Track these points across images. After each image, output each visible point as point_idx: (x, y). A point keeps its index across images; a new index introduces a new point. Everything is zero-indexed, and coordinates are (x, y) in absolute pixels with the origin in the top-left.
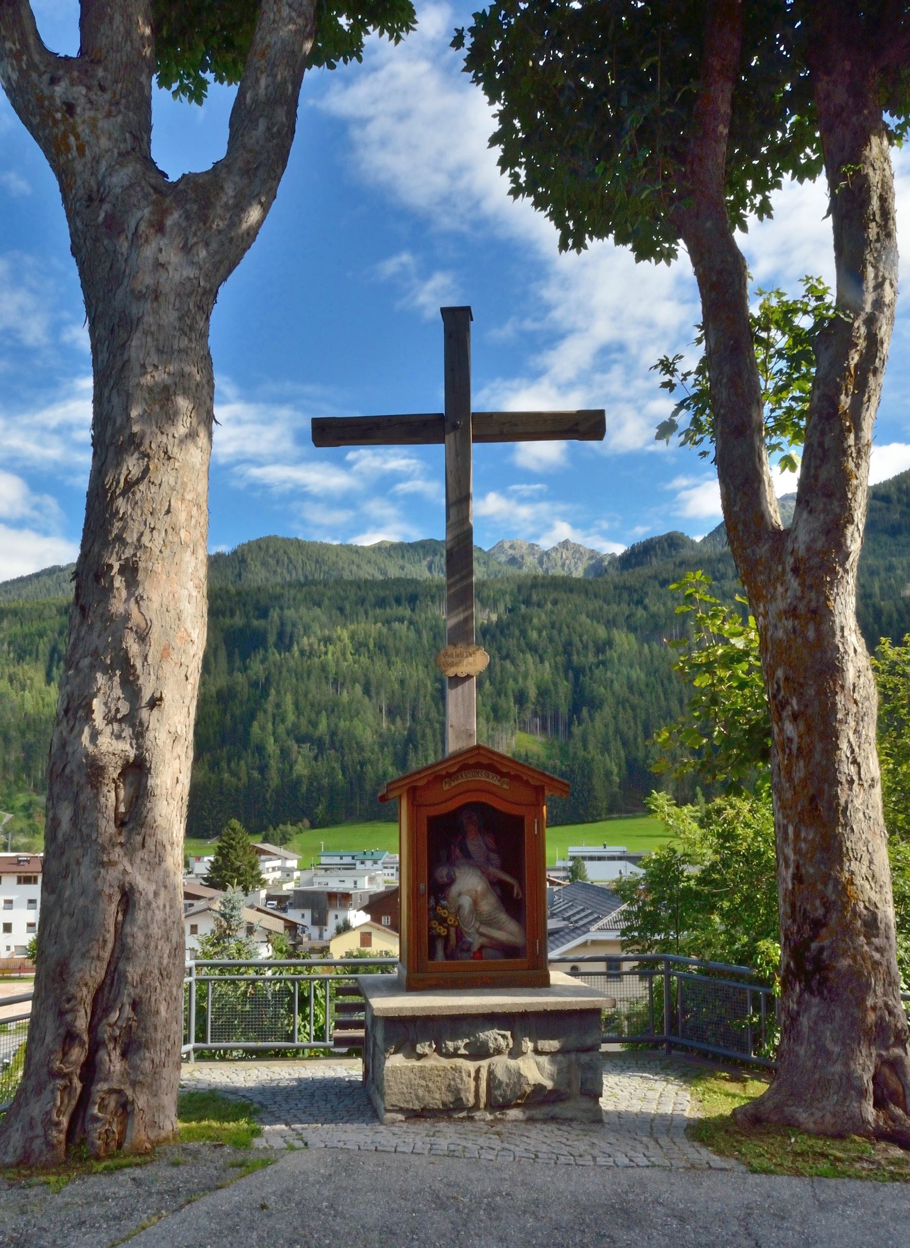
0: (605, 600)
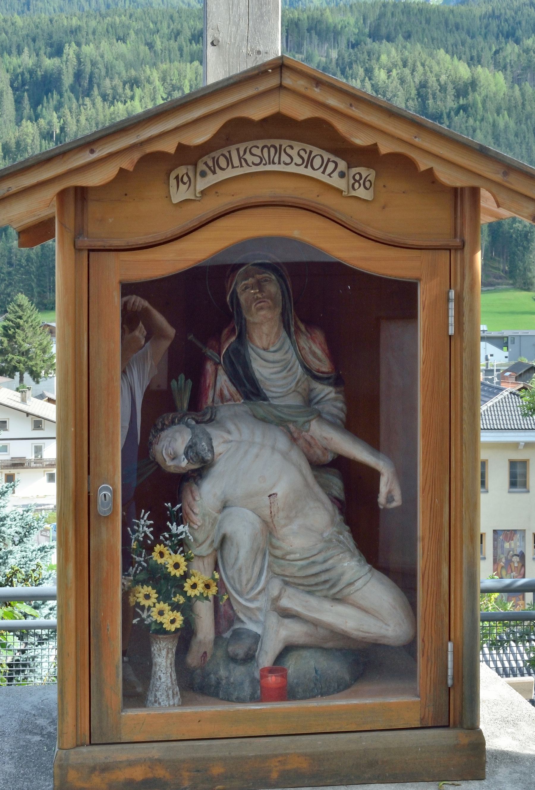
0: (468, 33)
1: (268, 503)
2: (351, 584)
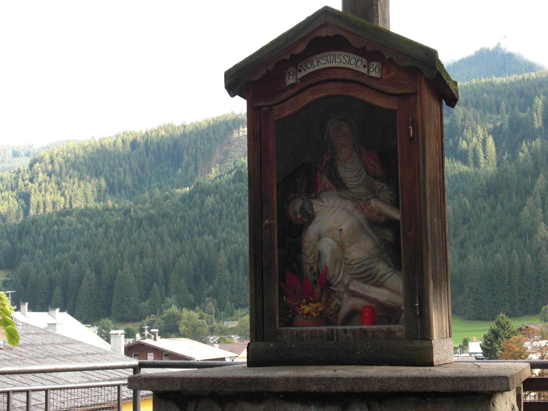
1: (338, 234)
2: (383, 276)
